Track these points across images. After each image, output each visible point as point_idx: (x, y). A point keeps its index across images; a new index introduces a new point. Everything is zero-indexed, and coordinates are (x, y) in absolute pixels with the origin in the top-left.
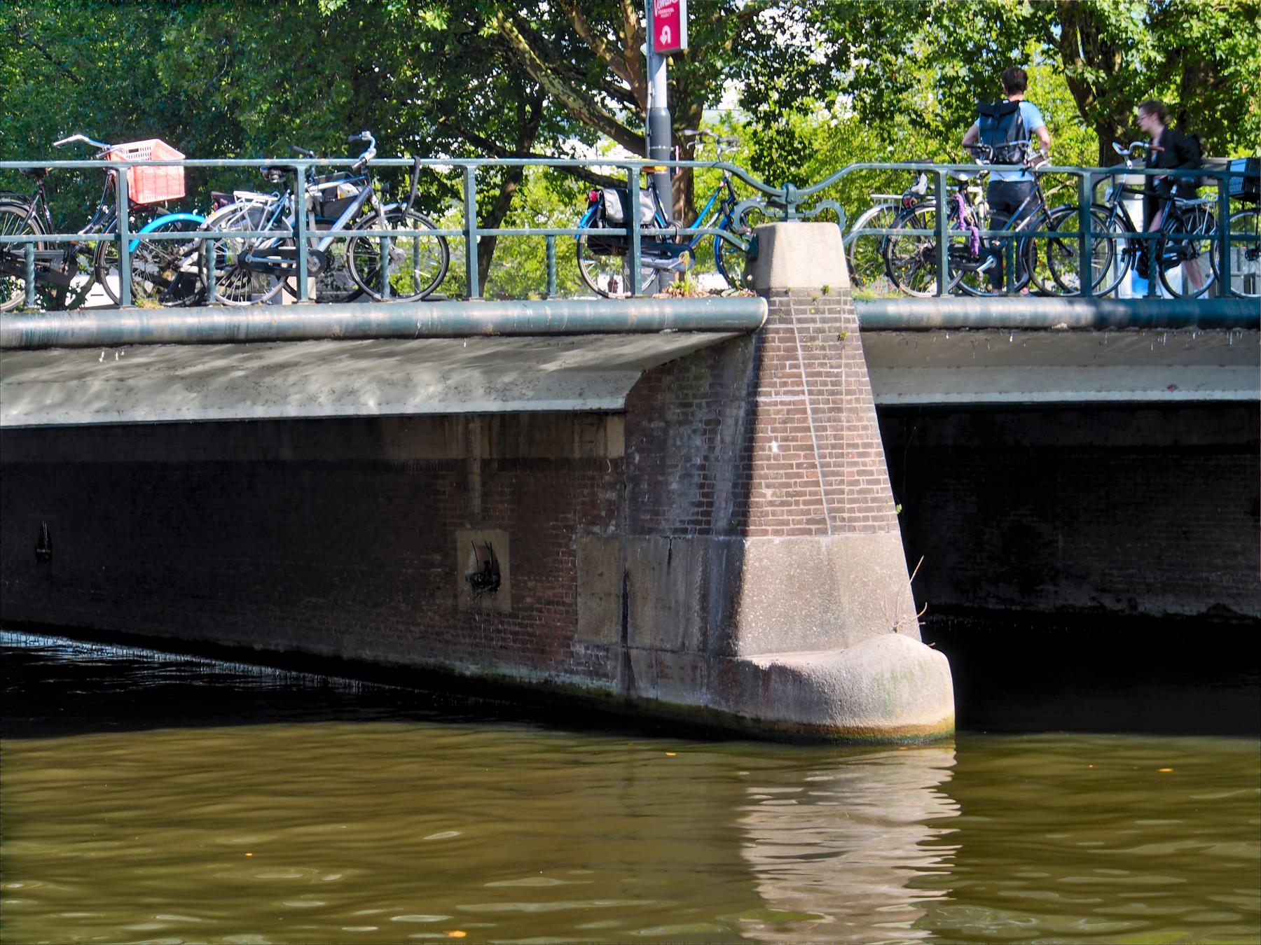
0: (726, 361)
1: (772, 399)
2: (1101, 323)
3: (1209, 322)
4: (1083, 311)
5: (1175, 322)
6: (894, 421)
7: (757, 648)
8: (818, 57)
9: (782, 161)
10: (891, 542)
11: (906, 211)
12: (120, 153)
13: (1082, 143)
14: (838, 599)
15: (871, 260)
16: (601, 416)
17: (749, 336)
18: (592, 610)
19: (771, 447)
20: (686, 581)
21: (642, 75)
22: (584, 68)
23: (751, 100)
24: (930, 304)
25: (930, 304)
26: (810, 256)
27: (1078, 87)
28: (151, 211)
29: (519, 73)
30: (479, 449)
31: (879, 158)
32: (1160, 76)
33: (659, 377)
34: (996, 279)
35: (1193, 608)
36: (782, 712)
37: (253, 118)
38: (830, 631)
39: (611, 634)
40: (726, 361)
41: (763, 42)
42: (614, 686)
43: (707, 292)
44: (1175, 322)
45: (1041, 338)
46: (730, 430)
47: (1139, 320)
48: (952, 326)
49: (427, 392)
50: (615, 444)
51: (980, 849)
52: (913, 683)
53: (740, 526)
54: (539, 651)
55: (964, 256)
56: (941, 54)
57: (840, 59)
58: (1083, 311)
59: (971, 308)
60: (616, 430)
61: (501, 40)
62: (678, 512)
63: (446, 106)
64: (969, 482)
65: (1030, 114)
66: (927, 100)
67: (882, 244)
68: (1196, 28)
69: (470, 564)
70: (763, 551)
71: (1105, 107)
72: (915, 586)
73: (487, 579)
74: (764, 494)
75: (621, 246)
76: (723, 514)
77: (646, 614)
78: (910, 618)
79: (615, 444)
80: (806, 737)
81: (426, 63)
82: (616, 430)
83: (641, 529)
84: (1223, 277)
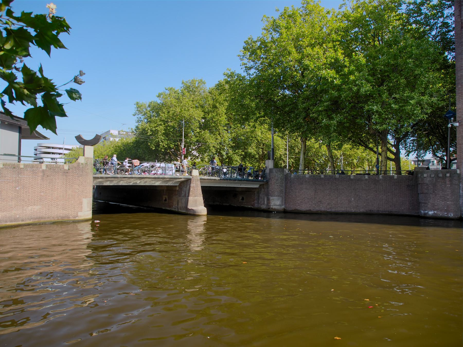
0: (188, 181)
1: (192, 185)
2: (221, 179)
3: (230, 180)
4: (219, 178)
5: (227, 180)
6: (203, 187)
7: (189, 207)
8: (197, 156)
9: (194, 165)
10: (202, 198)
11: (204, 169)
12: (133, 161)
13: (220, 164)
14: (196, 202)
15: (201, 173)
16: (176, 186)
17: (190, 179)
18: (175, 203)
19: (191, 189)
20: (183, 201)
21: (181, 156)
22: (176, 155)
23: (191, 159)
24: (206, 177)
25: (206, 177)
26: (195, 173)
27: (219, 159)
28: (136, 166)
29: (170, 155)
30: (165, 189)
31: (203, 164)
32: (226, 159)
33: (182, 183)
34: (212, 175)
35: (228, 205)
36: (192, 213)
37: (146, 158)
38: (196, 206)
39: (177, 205)
40: (188, 181)
41: (192, 154)
42: (177, 210)
43: (186, 175)
44: (227, 180)
45: (215, 181)
46: (188, 187)
47: (223, 180)
48: (208, 179)
49: (158, 183)
50: (178, 189)
51: (210, 230)
52: (202, 210)
53: (188, 196)
54: (170, 207)
55: (209, 173)
56: (208, 156)
57: (199, 156)
58: (219, 178)
59: (209, 178)
60: (178, 187)
61: (169, 152)
62: (183, 195)
63: (164, 158)
64: (209, 193)
65: (215, 161)
66: (206, 160)
67: (202, 172)
68: (229, 155)
69: (164, 199)
70: (190, 198)
71: (222, 161)
72: (47, 79)
73: (166, 200)
74: (191, 193)
75: (179, 171)
76: (187, 195)
77: (180, 204)
78: (203, 205)
79: (178, 189)
80: (193, 215)
81: (162, 154)
82: (178, 187)
83: (180, 196)
84: (231, 176)
